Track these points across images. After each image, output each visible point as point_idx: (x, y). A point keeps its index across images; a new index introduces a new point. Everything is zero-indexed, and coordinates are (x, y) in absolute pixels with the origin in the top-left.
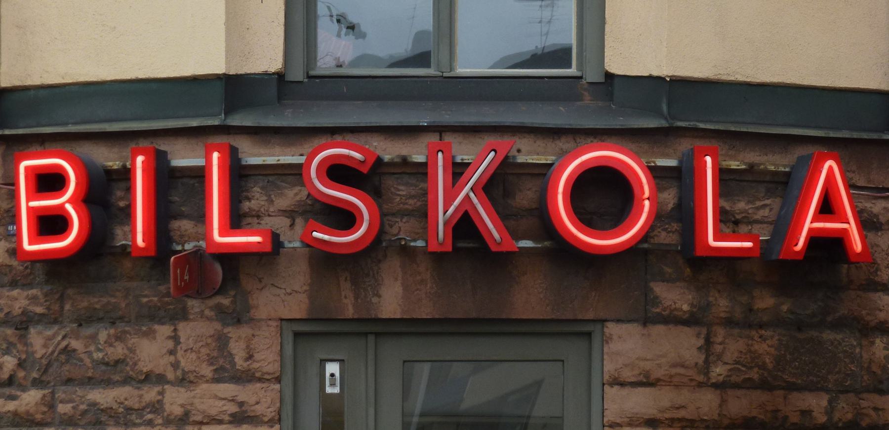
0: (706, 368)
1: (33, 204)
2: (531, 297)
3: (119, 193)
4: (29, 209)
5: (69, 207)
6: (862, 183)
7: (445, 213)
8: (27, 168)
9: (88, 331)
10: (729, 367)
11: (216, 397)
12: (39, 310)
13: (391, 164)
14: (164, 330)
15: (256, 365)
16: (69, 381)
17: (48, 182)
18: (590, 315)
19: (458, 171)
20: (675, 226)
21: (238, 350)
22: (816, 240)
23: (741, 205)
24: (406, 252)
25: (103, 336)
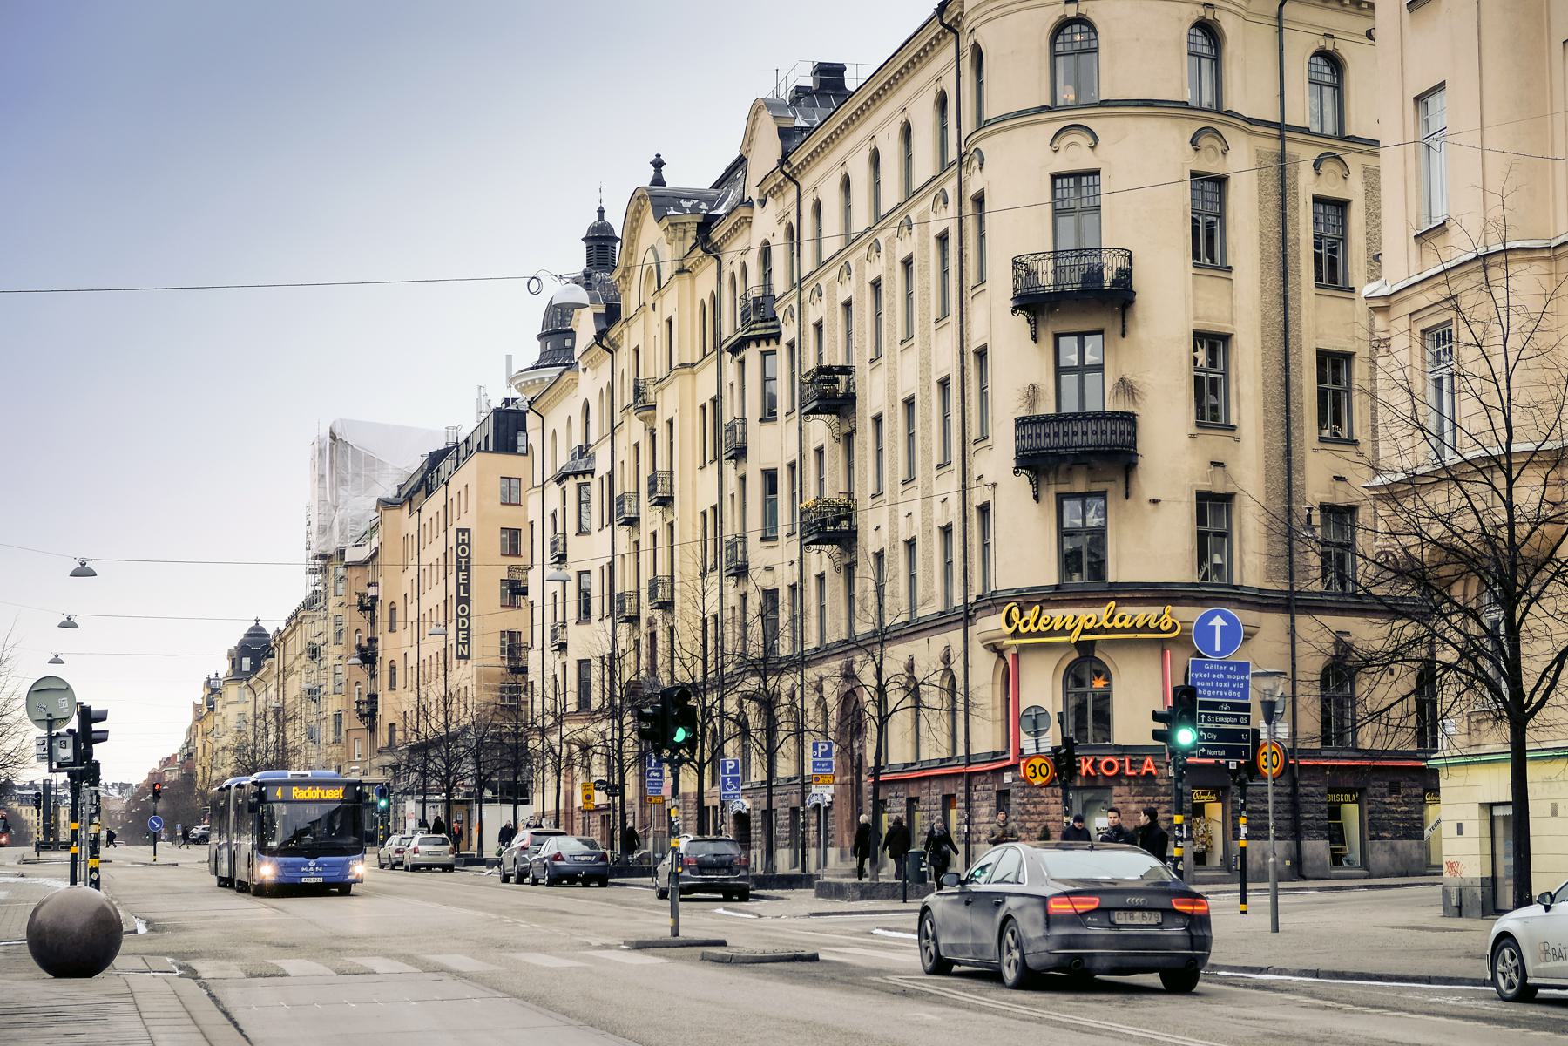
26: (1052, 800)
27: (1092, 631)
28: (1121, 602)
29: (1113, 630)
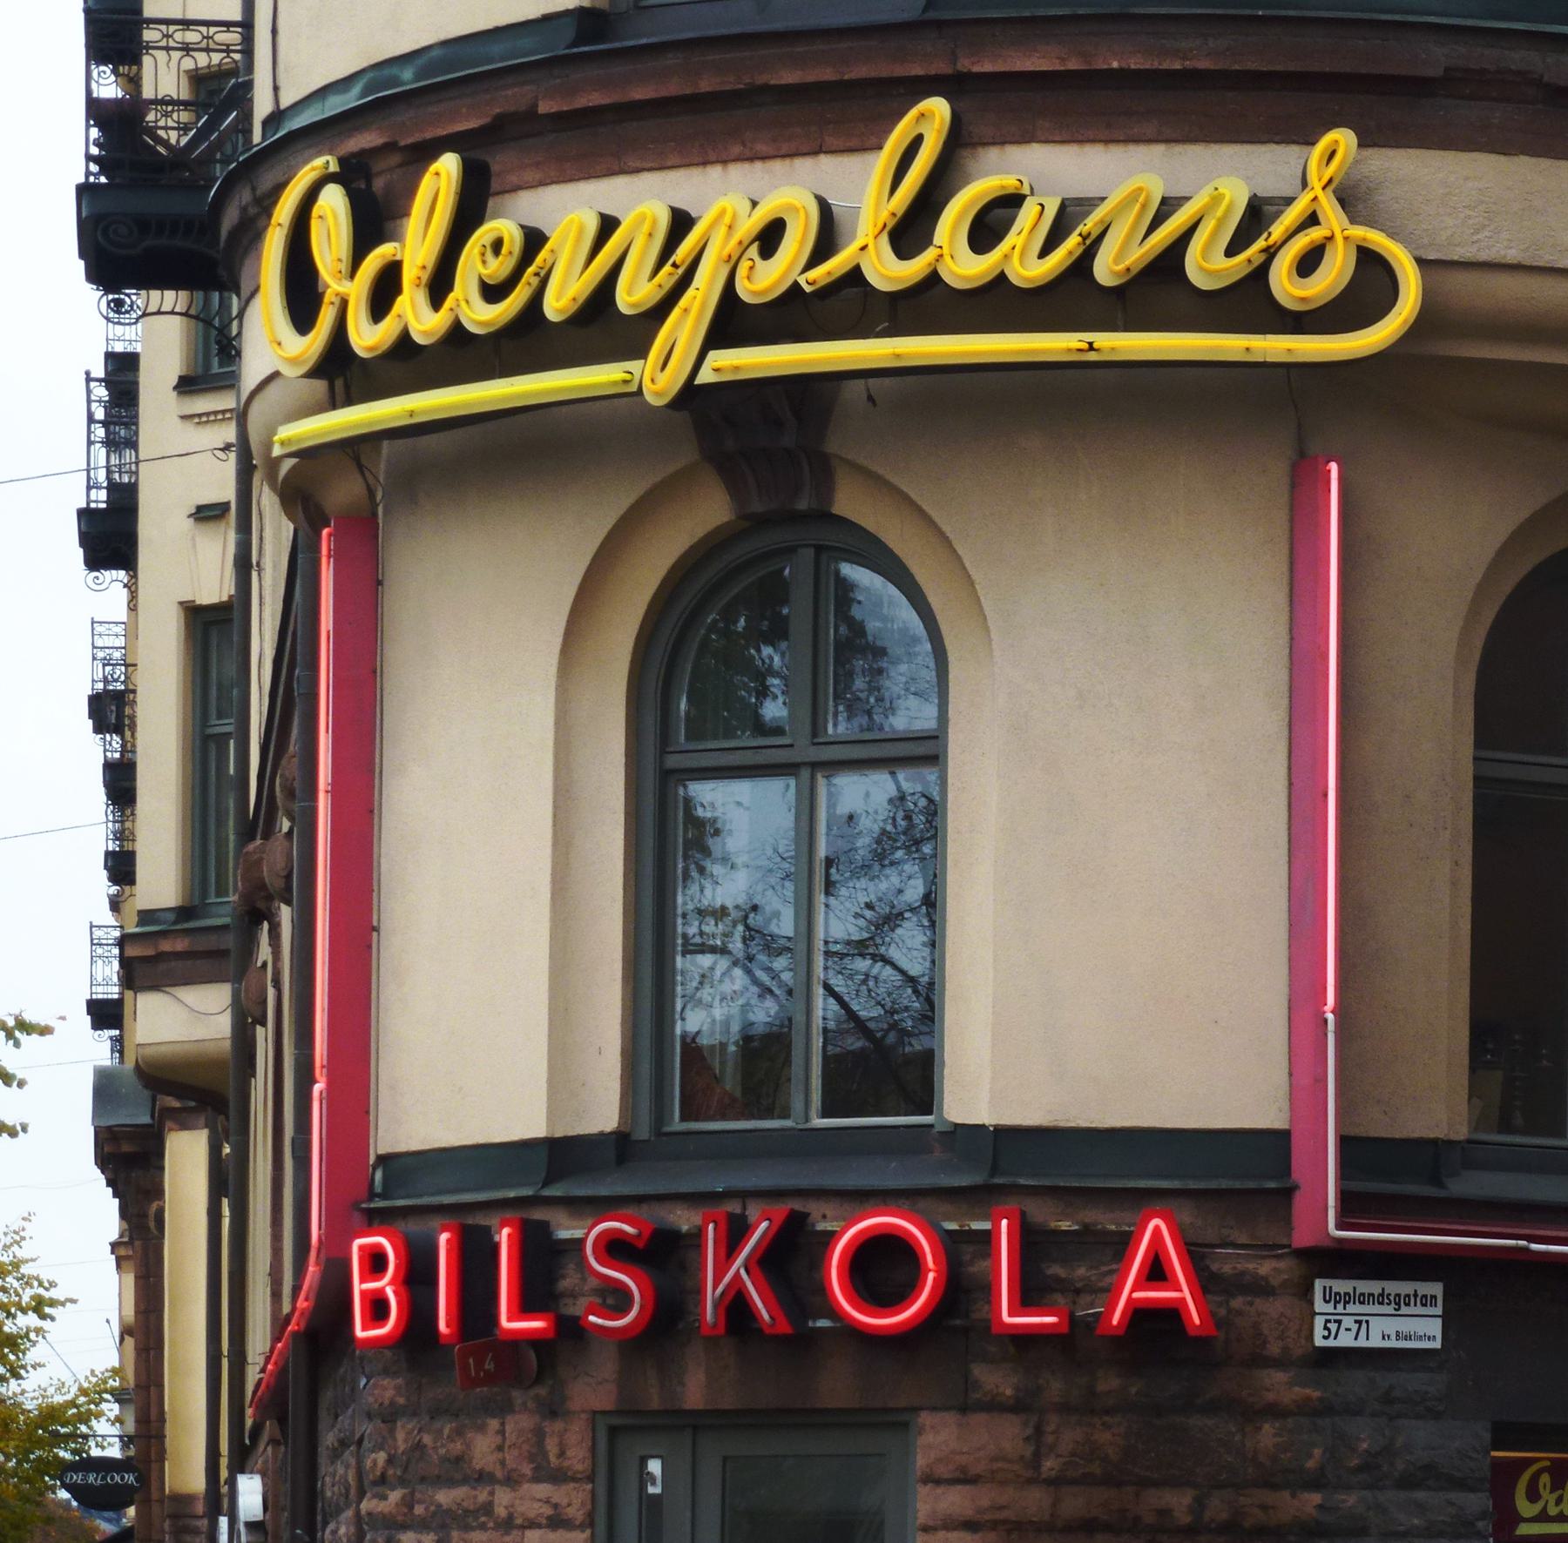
0: (1036, 1461)
2: (836, 1385)
4: (363, 1293)
7: (715, 1287)
8: (361, 1248)
9: (437, 1425)
10: (1061, 1460)
11: (534, 1499)
14: (494, 1424)
15: (566, 1464)
18: (903, 1403)
21: (551, 1446)
22: (1140, 1314)
26: (534, 1497)
27: (793, 315)
29: (929, 305)
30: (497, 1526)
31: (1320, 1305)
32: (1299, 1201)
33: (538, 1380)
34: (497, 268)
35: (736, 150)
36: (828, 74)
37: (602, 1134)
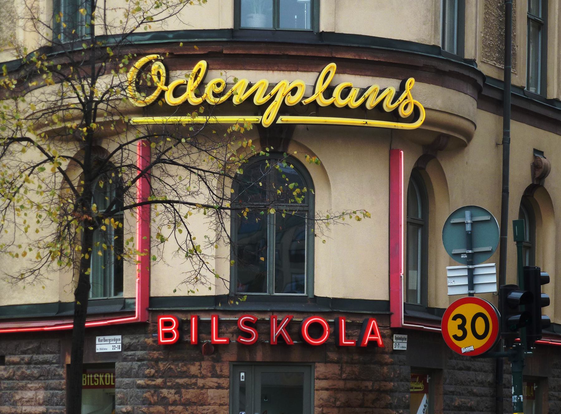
1: (163, 329)
2: (296, 356)
3: (185, 326)
5: (173, 331)
6: (381, 325)
9: (176, 363)
12: (162, 357)
13: (260, 320)
14: (197, 364)
16: (170, 377)
17: (168, 324)
18: (311, 361)
19: (279, 323)
20: (333, 337)
21: (218, 369)
22: (370, 341)
23: (350, 331)
24: (264, 344)
25: (180, 365)
26: (212, 381)
28: (345, 66)
29: (332, 110)
30: (198, 388)
31: (394, 340)
32: (392, 317)
33: (213, 353)
34: (218, 90)
35: (276, 68)
36: (303, 54)
37: (225, 295)
